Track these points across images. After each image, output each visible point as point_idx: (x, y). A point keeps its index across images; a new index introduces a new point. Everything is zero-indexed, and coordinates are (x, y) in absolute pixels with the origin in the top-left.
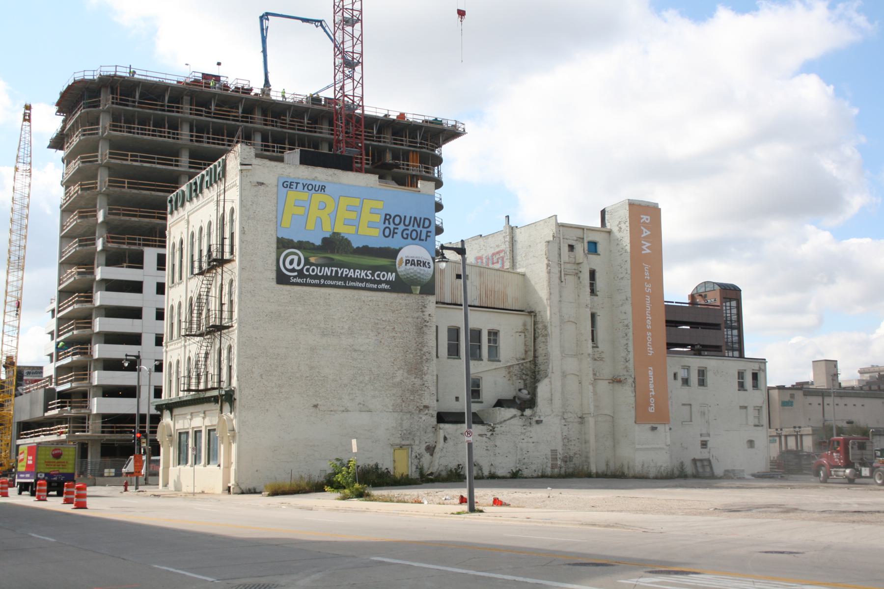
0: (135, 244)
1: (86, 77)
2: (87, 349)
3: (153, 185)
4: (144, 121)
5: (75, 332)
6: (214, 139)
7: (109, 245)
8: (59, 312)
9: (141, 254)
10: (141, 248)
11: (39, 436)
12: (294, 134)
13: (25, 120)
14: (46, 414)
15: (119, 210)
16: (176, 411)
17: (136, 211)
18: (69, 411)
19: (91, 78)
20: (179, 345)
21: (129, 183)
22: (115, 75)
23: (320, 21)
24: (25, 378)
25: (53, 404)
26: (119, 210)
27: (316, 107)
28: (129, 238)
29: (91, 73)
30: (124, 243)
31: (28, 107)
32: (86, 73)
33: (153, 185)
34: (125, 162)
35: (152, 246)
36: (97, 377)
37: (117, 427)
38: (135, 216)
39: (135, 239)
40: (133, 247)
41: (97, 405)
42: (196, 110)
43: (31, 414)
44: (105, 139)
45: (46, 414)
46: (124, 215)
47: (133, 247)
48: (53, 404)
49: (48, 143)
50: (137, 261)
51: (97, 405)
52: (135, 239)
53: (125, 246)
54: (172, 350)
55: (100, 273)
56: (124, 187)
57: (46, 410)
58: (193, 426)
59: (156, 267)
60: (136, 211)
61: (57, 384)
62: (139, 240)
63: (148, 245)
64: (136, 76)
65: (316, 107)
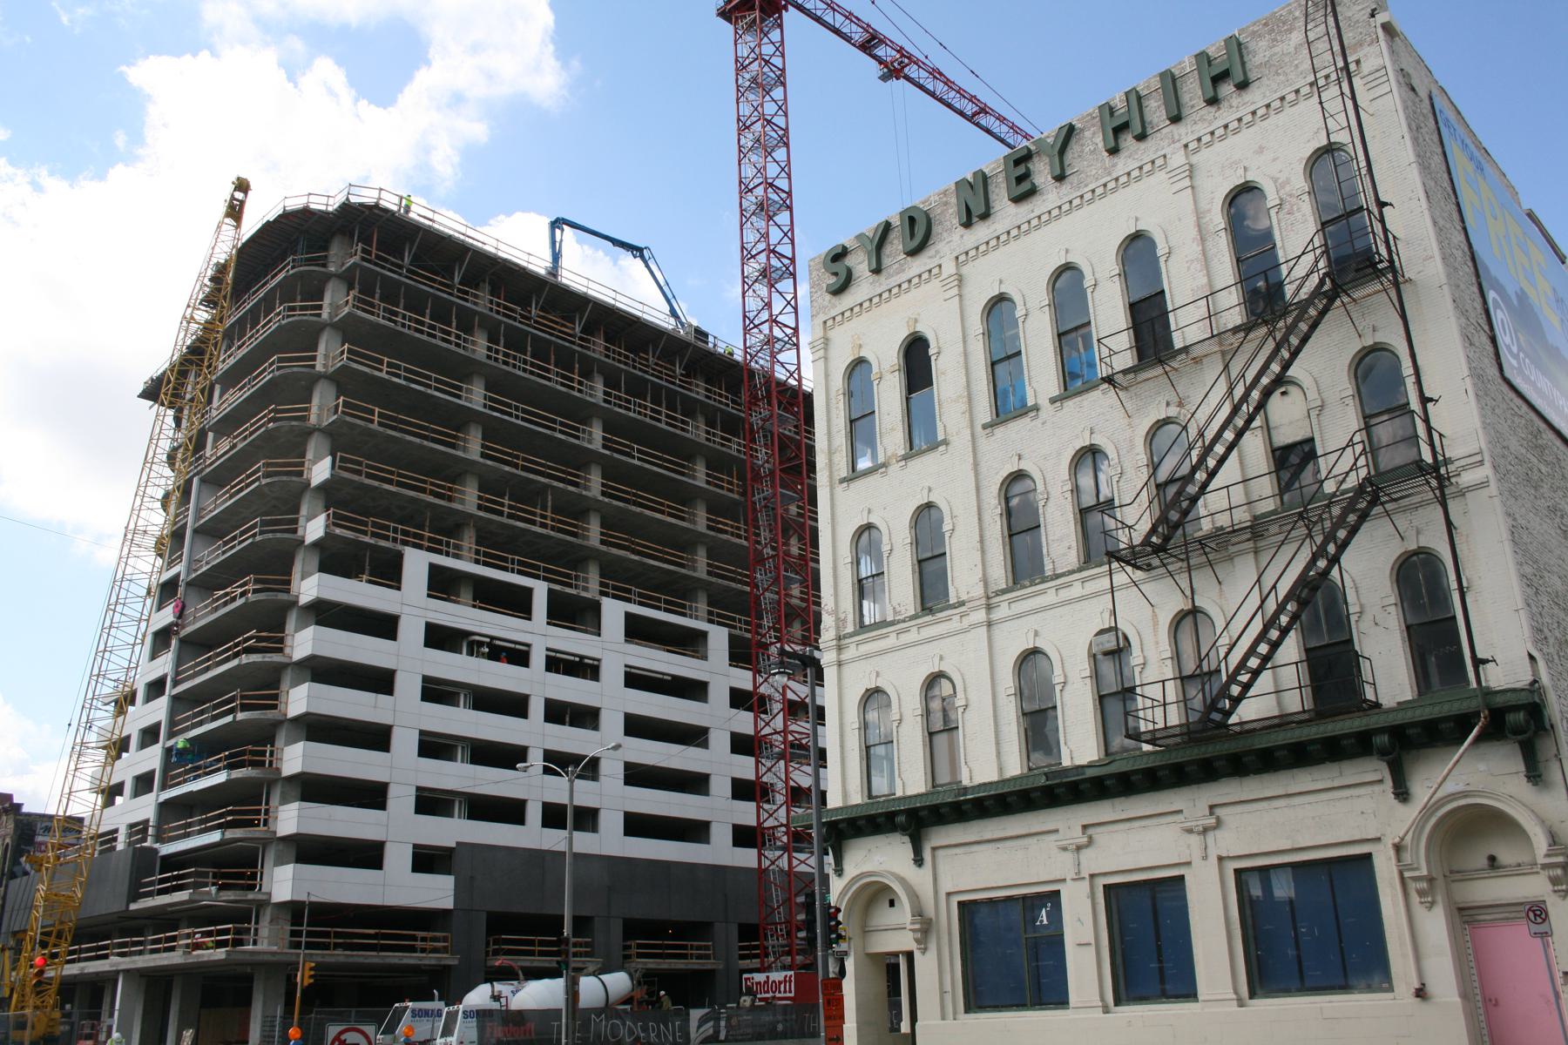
0: (386, 538)
1: (312, 206)
2: (263, 753)
3: (421, 427)
4: (416, 303)
5: (241, 716)
6: (533, 365)
7: (338, 531)
8: (176, 683)
9: (399, 557)
10: (399, 547)
11: (106, 957)
12: (662, 387)
13: (228, 215)
14: (133, 907)
15: (360, 464)
16: (939, 837)
17: (392, 473)
18: (212, 895)
19: (323, 208)
20: (1091, 587)
21: (380, 415)
22: (377, 206)
23: (640, 250)
24: (39, 839)
25: (151, 884)
26: (360, 464)
27: (700, 344)
28: (375, 525)
29: (324, 200)
30: (365, 533)
31: (242, 186)
32: (312, 199)
33: (421, 427)
34: (377, 373)
35: (420, 547)
36: (290, 818)
37: (337, 935)
38: (390, 482)
39: (387, 528)
40: (383, 543)
41: (283, 882)
42: (506, 308)
43: (1001, 769)
44: (335, 326)
45: (133, 907)
46: (369, 476)
47: (383, 543)
48: (151, 884)
49: (140, 390)
50: (389, 573)
51: (283, 882)
52: (387, 528)
53: (367, 539)
54: (853, 660)
55: (310, 586)
56: (372, 421)
57: (135, 896)
58: (947, 885)
59: (425, 591)
60: (392, 473)
61: (159, 838)
62: (395, 530)
63: (416, 546)
64: (412, 215)
65: (700, 344)
